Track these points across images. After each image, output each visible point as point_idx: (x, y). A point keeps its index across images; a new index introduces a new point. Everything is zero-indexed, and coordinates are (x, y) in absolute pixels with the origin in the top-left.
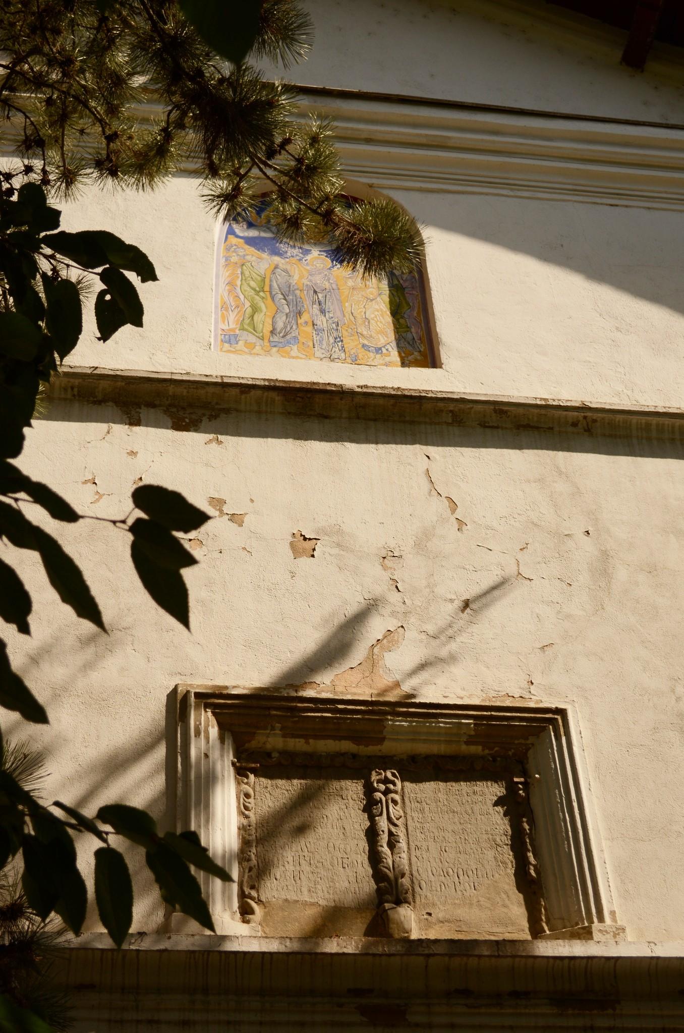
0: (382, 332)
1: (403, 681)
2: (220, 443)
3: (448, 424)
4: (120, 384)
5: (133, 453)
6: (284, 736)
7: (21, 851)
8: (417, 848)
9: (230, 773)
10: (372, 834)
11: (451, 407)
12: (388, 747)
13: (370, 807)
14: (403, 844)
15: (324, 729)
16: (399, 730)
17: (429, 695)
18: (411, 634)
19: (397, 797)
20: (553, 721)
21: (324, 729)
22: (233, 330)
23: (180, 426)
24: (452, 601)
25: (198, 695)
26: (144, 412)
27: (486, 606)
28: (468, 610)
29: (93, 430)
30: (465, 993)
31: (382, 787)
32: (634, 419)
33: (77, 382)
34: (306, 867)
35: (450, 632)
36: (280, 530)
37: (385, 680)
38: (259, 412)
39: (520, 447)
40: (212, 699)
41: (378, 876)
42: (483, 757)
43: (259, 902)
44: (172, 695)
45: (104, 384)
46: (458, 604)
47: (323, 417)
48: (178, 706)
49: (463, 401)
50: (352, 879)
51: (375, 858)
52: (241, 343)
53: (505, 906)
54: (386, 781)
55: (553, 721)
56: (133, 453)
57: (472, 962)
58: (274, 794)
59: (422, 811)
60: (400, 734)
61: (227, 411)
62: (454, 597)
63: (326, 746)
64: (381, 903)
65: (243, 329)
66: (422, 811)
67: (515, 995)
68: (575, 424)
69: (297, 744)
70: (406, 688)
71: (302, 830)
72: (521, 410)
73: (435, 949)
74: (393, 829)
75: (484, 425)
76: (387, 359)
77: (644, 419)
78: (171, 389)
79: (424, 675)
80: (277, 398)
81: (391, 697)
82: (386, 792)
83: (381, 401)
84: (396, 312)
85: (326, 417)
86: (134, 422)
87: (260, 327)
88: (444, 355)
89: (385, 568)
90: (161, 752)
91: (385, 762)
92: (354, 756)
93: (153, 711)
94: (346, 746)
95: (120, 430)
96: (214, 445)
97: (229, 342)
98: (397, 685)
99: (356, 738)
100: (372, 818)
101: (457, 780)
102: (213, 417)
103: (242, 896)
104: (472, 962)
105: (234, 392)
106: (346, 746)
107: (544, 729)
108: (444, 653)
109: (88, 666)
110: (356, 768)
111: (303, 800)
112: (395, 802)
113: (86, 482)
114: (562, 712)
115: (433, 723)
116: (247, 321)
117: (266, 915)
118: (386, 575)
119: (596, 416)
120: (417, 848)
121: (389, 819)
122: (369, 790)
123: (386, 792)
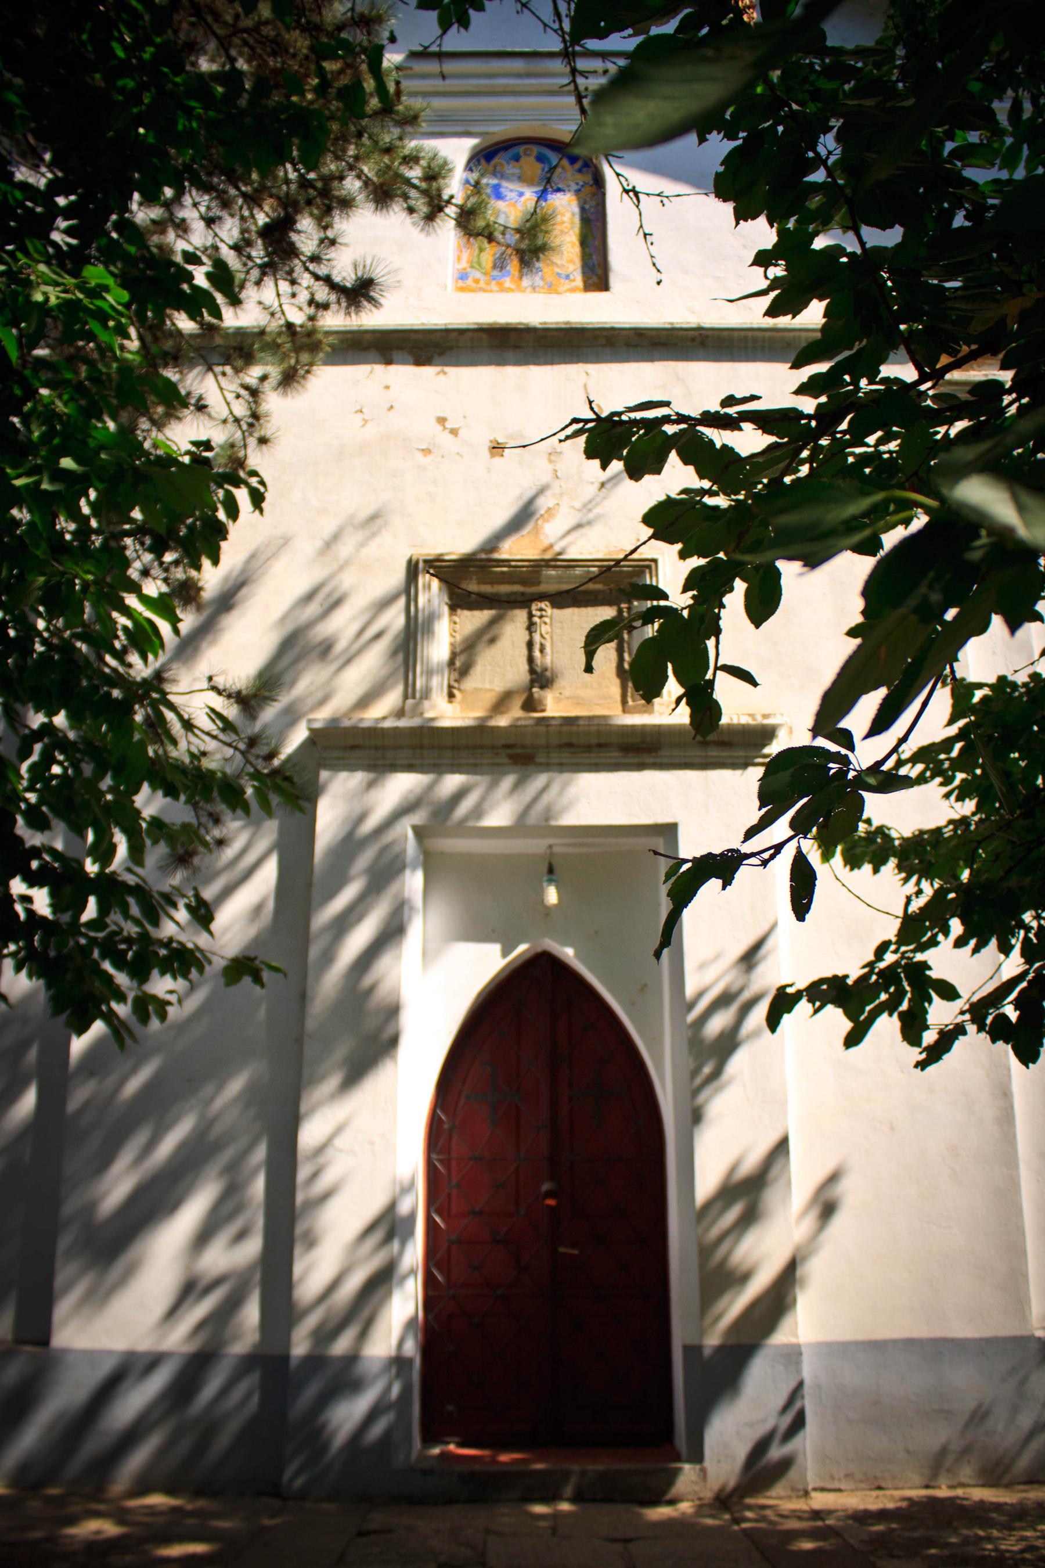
0: (571, 261)
1: (556, 543)
2: (445, 373)
3: (603, 346)
4: (378, 335)
5: (387, 387)
6: (478, 583)
7: (805, 179)
8: (558, 652)
9: (446, 610)
10: (530, 645)
11: (605, 333)
12: (543, 588)
13: (531, 627)
14: (548, 650)
15: (503, 579)
16: (550, 577)
17: (571, 554)
18: (564, 509)
19: (547, 620)
20: (649, 567)
21: (503, 579)
22: (465, 269)
23: (419, 362)
24: (592, 483)
25: (426, 561)
26: (396, 355)
27: (616, 485)
28: (603, 490)
29: (361, 370)
30: (570, 745)
31: (538, 613)
32: (736, 334)
33: (349, 336)
34: (488, 667)
35: (590, 506)
36: (483, 439)
37: (546, 542)
38: (472, 348)
39: (652, 360)
40: (436, 566)
41: (532, 671)
42: (603, 591)
43: (459, 689)
44: (410, 561)
45: (368, 336)
46: (597, 485)
47: (517, 347)
48: (413, 570)
49: (613, 329)
50: (517, 673)
51: (531, 660)
52: (470, 279)
53: (607, 687)
54: (541, 610)
55: (649, 567)
56: (387, 387)
57: (574, 728)
58: (473, 620)
59: (562, 628)
60: (551, 581)
61: (451, 348)
62: (593, 480)
63: (505, 589)
64: (530, 689)
65: (472, 267)
66: (562, 628)
67: (600, 746)
68: (693, 340)
69: (487, 589)
70: (557, 548)
71: (493, 641)
72: (654, 333)
73: (553, 722)
74: (543, 641)
75: (628, 345)
76: (573, 284)
77: (743, 333)
78: (413, 336)
79: (569, 538)
80: (484, 336)
81: (548, 556)
82: (541, 617)
83: (555, 333)
84: (583, 242)
85: (519, 347)
86: (389, 362)
87: (484, 263)
88: (614, 280)
89: (550, 461)
90: (402, 602)
91: (541, 597)
92: (523, 594)
93: (397, 576)
94: (518, 588)
95: (379, 369)
96: (441, 376)
97: (461, 279)
98: (551, 546)
99: (523, 582)
100: (531, 633)
101: (586, 606)
102: (442, 353)
103: (450, 687)
104: (574, 728)
105: (454, 335)
106: (518, 588)
107: (643, 572)
108: (591, 516)
109: (362, 545)
110: (524, 602)
111: (493, 622)
112: (545, 623)
113: (356, 412)
114: (655, 561)
115: (571, 572)
116: (475, 260)
117: (464, 699)
118: (550, 467)
119: (710, 333)
120: (558, 652)
121: (542, 636)
122: (531, 616)
123: (541, 617)
